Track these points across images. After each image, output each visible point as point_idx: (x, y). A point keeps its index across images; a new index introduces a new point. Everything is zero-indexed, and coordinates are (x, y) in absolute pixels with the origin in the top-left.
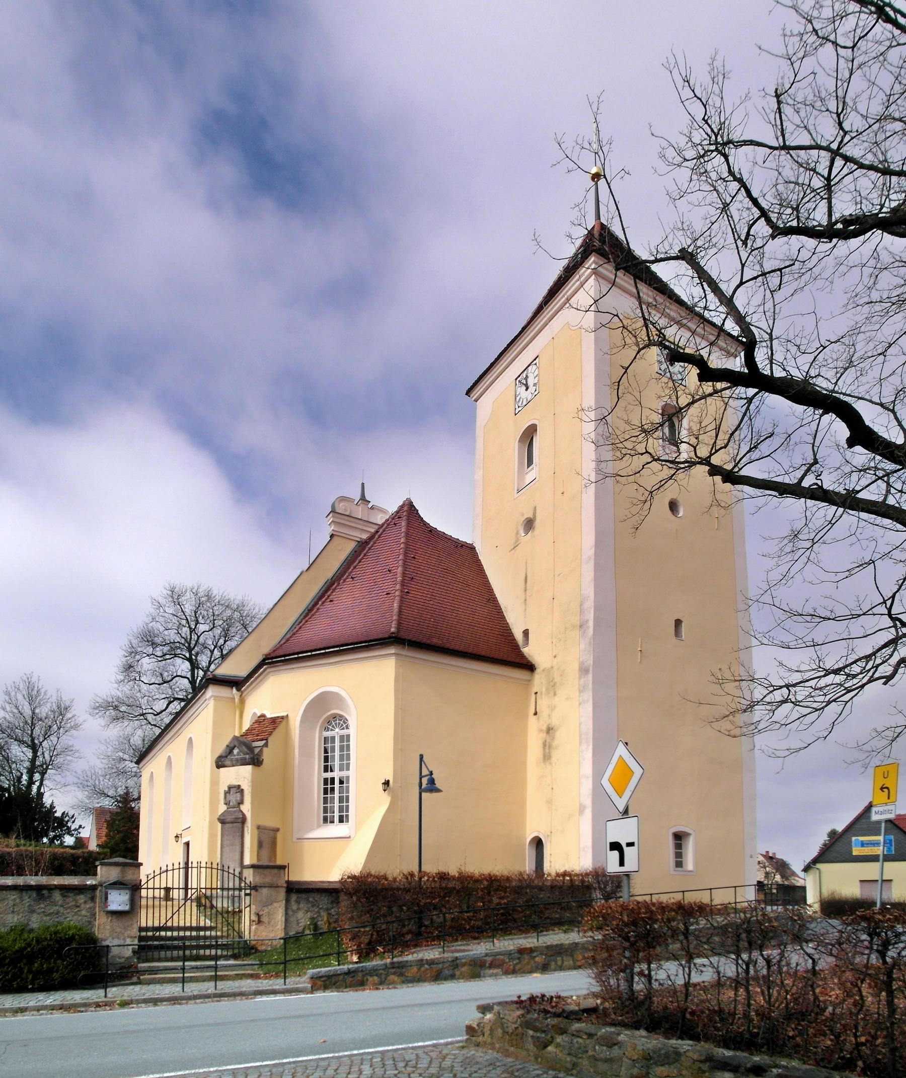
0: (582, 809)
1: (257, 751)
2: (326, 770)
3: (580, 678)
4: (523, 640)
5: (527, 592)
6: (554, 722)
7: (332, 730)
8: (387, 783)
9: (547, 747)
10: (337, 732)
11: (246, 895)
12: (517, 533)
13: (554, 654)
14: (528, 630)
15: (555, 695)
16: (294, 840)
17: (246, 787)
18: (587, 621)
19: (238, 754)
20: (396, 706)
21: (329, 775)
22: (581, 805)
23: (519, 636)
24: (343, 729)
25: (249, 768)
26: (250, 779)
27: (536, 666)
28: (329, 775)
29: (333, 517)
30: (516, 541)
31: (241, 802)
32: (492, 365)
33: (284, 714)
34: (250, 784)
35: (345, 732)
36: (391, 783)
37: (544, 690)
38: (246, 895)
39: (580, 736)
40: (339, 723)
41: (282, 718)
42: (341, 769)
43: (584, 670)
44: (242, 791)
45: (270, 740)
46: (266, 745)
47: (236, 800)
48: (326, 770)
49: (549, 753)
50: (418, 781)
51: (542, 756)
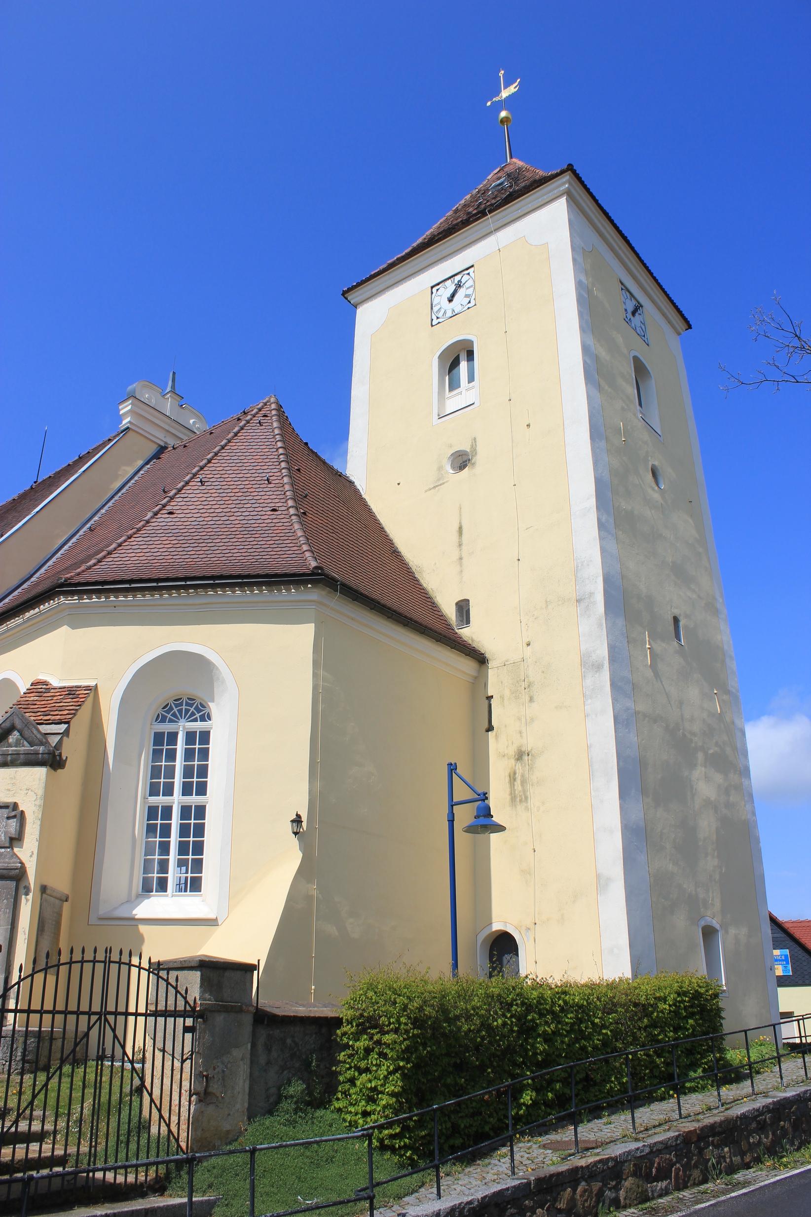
0: (602, 883)
1: (54, 740)
2: (154, 791)
3: (583, 677)
4: (456, 620)
5: (464, 547)
6: (530, 742)
7: (171, 721)
8: (298, 820)
9: (518, 781)
10: (183, 727)
11: (186, 1029)
12: (440, 468)
13: (526, 640)
14: (467, 601)
15: (531, 699)
16: (93, 920)
17: (31, 807)
18: (591, 594)
19: (17, 744)
20: (315, 688)
21: (160, 800)
22: (598, 876)
23: (450, 611)
24: (195, 720)
25: (41, 772)
26: (41, 792)
27: (487, 655)
28: (160, 800)
29: (132, 404)
30: (439, 480)
31: (16, 839)
32: (587, 190)
33: (92, 683)
34: (40, 802)
35: (198, 726)
36: (304, 818)
37: (507, 693)
38: (186, 1029)
39: (590, 765)
40: (187, 711)
41: (88, 688)
42: (187, 790)
43: (588, 665)
44: (22, 817)
45: (71, 723)
46: (66, 733)
47: (6, 833)
48: (154, 791)
49: (524, 791)
50: (446, 810)
51: (508, 798)
